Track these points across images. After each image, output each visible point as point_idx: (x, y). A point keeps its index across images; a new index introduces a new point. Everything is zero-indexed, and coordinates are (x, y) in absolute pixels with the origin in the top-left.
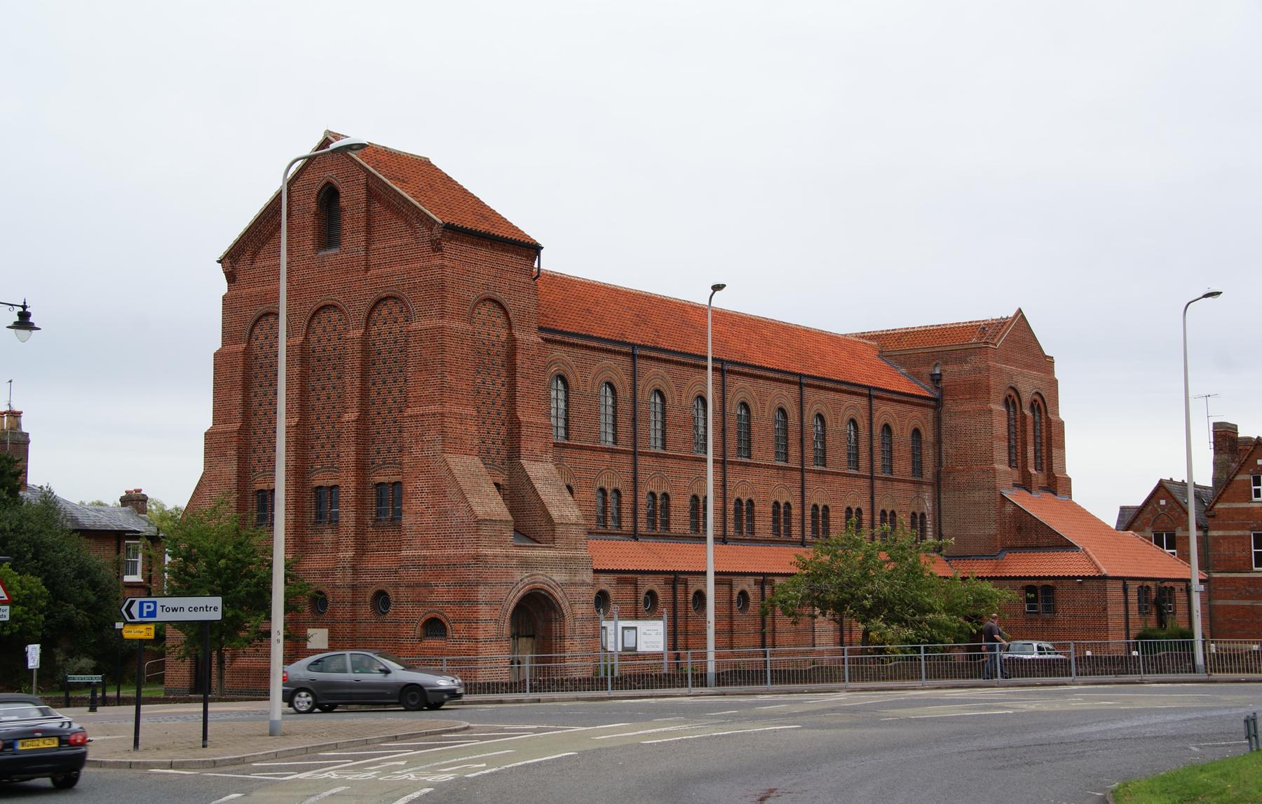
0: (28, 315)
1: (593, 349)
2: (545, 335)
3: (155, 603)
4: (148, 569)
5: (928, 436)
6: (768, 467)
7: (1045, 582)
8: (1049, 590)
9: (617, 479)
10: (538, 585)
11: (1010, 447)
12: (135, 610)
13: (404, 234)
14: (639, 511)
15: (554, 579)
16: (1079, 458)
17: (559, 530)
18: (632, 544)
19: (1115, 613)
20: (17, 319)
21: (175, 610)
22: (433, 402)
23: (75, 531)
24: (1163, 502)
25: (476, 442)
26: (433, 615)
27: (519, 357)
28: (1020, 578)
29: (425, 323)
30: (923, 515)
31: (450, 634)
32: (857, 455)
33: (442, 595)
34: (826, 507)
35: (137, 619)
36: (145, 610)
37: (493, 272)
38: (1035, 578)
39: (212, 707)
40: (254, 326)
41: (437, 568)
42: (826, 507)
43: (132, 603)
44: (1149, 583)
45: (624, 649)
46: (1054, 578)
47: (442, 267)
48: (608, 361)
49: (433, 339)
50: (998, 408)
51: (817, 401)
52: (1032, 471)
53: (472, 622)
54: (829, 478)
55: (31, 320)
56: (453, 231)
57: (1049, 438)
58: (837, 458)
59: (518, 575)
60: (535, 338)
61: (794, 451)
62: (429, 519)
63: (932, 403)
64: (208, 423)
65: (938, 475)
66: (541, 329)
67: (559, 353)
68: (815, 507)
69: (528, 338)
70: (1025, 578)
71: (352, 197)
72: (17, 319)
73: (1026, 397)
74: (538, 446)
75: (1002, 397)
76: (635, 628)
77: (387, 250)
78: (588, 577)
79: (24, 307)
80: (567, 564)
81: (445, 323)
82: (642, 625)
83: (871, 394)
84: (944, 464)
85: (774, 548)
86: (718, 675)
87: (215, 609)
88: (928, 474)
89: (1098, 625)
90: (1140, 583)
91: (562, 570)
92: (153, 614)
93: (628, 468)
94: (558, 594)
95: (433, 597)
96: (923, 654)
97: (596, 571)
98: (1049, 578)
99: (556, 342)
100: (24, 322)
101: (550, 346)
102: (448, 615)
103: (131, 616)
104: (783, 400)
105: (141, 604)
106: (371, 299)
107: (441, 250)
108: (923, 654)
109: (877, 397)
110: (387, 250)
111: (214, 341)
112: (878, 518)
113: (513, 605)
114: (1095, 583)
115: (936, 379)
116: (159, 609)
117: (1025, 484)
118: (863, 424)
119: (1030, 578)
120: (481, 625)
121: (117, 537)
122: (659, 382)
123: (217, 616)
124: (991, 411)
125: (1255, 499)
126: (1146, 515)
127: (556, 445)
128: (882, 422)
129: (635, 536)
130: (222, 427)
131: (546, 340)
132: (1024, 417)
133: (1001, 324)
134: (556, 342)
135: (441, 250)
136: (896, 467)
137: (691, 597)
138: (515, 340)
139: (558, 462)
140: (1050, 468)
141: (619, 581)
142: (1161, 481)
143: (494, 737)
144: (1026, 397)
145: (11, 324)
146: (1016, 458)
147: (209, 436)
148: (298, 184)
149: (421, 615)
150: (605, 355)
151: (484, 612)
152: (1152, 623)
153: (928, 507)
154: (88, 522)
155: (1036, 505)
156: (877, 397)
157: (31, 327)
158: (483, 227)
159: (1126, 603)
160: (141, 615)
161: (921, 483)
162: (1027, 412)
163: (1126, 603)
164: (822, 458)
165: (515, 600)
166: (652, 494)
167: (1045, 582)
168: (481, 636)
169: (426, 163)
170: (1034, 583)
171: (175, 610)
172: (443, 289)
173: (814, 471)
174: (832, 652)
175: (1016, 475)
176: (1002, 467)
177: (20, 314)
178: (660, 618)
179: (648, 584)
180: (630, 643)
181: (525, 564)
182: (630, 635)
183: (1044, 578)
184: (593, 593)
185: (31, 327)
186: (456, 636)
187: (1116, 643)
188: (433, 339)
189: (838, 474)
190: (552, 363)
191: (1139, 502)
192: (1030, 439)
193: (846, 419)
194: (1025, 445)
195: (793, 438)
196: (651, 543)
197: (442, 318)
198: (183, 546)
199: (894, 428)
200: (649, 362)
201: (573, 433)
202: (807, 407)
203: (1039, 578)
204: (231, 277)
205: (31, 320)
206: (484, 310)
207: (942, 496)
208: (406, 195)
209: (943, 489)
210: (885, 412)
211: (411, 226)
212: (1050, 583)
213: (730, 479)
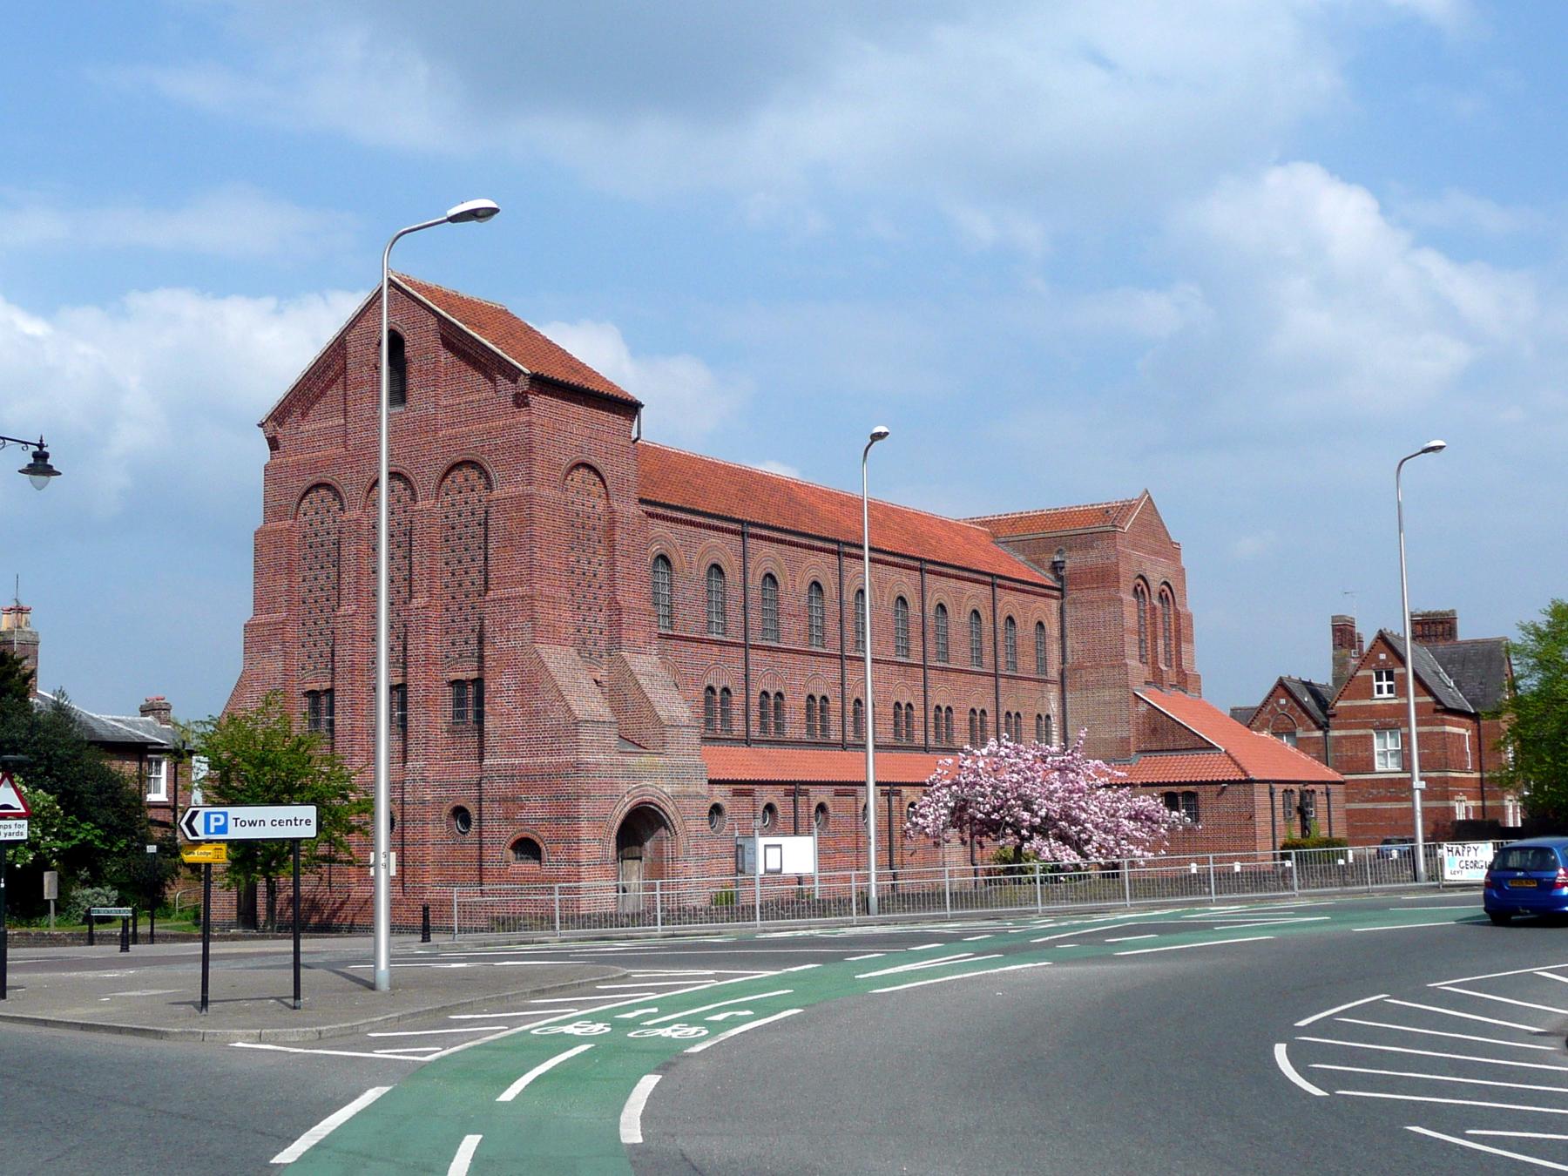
0: (46, 456)
1: (699, 525)
2: (645, 507)
3: (225, 814)
4: (174, 789)
5: (1053, 629)
6: (888, 662)
7: (1185, 788)
8: (1191, 796)
9: (725, 675)
10: (647, 799)
11: (1141, 641)
12: (198, 823)
13: (482, 387)
14: (751, 713)
15: (661, 791)
16: (1202, 656)
17: (670, 733)
18: (743, 750)
19: (1262, 818)
20: (32, 461)
21: (253, 823)
22: (521, 583)
23: (91, 743)
24: (1283, 701)
25: (571, 630)
26: (524, 834)
27: (618, 531)
28: (1159, 784)
29: (511, 490)
30: (1048, 717)
31: (545, 856)
32: (980, 650)
33: (534, 816)
34: (949, 709)
35: (202, 836)
36: (213, 824)
37: (587, 432)
38: (1174, 784)
39: (215, 948)
40: (302, 499)
41: (528, 778)
42: (949, 709)
43: (194, 814)
44: (1292, 786)
45: (766, 871)
46: (1196, 783)
47: (530, 424)
48: (715, 539)
49: (519, 509)
50: (1128, 598)
51: (940, 589)
52: (1164, 668)
53: (572, 842)
54: (953, 676)
55: (49, 462)
56: (544, 385)
57: (1178, 631)
58: (960, 655)
59: (625, 785)
60: (635, 510)
61: (916, 646)
62: (518, 721)
63: (1056, 593)
64: (247, 613)
65: (1062, 674)
66: (642, 501)
67: (659, 528)
68: (938, 708)
69: (630, 510)
70: (1164, 784)
71: (423, 345)
72: (32, 461)
73: (1155, 586)
74: (641, 636)
75: (1132, 586)
76: (780, 846)
77: (463, 407)
78: (703, 788)
79: (41, 446)
80: (676, 774)
81: (533, 489)
82: (789, 842)
83: (995, 581)
84: (1069, 660)
85: (896, 754)
86: (880, 900)
87: (308, 822)
88: (1054, 673)
89: (1243, 836)
90: (1285, 786)
91: (675, 777)
92: (222, 829)
93: (740, 664)
94: (670, 809)
95: (523, 814)
96: (557, 897)
97: (711, 782)
98: (1191, 783)
99: (657, 516)
100: (40, 465)
101: (650, 521)
102: (541, 835)
103: (194, 833)
104: (904, 588)
105: (207, 815)
106: (444, 464)
107: (527, 405)
108: (557, 897)
109: (999, 586)
110: (463, 407)
111: (256, 518)
112: (1002, 720)
113: (619, 822)
114: (1241, 787)
115: (1056, 567)
116: (231, 823)
117: (1157, 681)
118: (985, 615)
119: (1169, 784)
120: (583, 845)
121: (139, 750)
122: (770, 564)
123: (310, 831)
124: (1121, 600)
125: (1377, 696)
126: (1265, 715)
127: (660, 636)
128: (1005, 614)
129: (747, 741)
130: (263, 618)
131: (650, 515)
132: (1154, 609)
133: (1127, 507)
134: (657, 516)
135: (527, 405)
136: (1020, 665)
137: (813, 809)
138: (613, 512)
139: (662, 654)
140: (1179, 665)
141: (736, 793)
142: (1281, 679)
143: (671, 988)
144: (1155, 586)
145: (24, 466)
146: (1147, 656)
147: (248, 628)
148: (355, 332)
149: (512, 833)
150: (712, 533)
151: (585, 830)
152: (1297, 834)
153: (1054, 708)
154: (107, 735)
155: (1171, 705)
156: (999, 586)
157: (49, 471)
158: (575, 380)
159: (1273, 809)
160: (207, 831)
161: (1046, 681)
162: (1156, 602)
163: (1273, 809)
164: (944, 654)
165: (622, 817)
166: (765, 693)
167: (1185, 788)
168: (583, 860)
169: (506, 312)
170: (1174, 789)
171: (253, 823)
172: (530, 451)
173: (936, 668)
174: (963, 873)
175: (1146, 673)
176: (1133, 663)
177: (35, 455)
178: (810, 834)
179: (767, 795)
180: (773, 864)
181: (632, 775)
182: (773, 854)
183: (1185, 783)
184: (708, 806)
185: (49, 471)
186: (553, 859)
187: (1264, 856)
188: (519, 509)
189: (961, 671)
190: (654, 540)
191: (1257, 703)
192: (1160, 633)
193: (969, 610)
194: (1155, 639)
195: (915, 630)
196: (765, 750)
197: (530, 484)
198: (225, 756)
199: (1017, 621)
200: (761, 542)
201: (679, 622)
202: (928, 595)
203: (1180, 784)
204: (273, 444)
205: (49, 462)
206: (580, 474)
207: (1068, 695)
208: (485, 342)
209: (1068, 688)
210: (1009, 602)
211: (493, 380)
212: (1191, 788)
213: (848, 676)
